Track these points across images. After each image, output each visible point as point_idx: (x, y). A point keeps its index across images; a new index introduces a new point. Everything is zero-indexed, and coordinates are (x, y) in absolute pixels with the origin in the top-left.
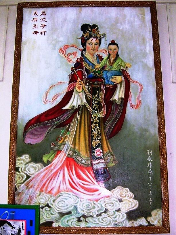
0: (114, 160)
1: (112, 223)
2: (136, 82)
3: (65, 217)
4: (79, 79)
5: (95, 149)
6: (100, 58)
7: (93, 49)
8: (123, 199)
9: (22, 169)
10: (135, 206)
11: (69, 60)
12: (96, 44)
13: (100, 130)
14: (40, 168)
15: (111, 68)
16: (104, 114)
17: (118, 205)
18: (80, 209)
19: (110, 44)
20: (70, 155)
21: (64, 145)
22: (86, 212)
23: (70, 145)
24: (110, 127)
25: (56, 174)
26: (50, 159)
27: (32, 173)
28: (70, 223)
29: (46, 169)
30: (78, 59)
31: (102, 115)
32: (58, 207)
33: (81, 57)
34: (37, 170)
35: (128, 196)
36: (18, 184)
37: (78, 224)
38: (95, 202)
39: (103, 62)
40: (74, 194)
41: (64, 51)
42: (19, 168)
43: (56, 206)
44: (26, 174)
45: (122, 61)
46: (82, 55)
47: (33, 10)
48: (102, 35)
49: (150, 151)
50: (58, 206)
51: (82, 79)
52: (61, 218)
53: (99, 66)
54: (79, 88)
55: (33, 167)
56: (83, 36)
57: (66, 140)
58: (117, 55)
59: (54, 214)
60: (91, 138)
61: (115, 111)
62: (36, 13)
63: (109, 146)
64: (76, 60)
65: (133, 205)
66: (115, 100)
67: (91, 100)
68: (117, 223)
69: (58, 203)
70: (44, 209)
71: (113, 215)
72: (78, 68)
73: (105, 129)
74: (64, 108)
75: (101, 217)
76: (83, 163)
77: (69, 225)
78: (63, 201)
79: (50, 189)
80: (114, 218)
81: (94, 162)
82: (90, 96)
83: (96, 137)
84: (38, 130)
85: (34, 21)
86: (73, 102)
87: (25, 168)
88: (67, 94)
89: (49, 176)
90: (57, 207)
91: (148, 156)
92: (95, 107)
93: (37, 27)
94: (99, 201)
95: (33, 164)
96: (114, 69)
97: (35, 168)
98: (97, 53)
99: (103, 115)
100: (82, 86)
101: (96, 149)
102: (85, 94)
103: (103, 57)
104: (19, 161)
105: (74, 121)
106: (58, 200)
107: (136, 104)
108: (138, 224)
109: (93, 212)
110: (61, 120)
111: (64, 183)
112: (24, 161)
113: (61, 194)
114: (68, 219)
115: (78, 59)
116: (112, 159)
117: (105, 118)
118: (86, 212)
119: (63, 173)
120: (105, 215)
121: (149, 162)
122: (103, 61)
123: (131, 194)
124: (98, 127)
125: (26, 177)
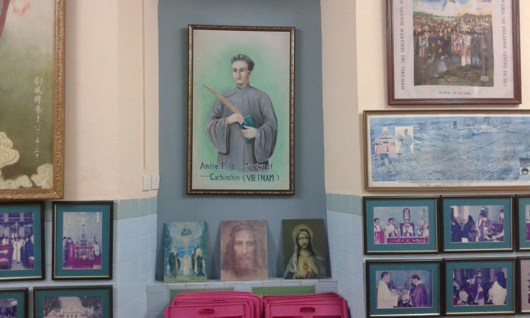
10: (13, 159)
35: (4, 144)
49: (39, 80)
65: (11, 158)
121: (37, 95)
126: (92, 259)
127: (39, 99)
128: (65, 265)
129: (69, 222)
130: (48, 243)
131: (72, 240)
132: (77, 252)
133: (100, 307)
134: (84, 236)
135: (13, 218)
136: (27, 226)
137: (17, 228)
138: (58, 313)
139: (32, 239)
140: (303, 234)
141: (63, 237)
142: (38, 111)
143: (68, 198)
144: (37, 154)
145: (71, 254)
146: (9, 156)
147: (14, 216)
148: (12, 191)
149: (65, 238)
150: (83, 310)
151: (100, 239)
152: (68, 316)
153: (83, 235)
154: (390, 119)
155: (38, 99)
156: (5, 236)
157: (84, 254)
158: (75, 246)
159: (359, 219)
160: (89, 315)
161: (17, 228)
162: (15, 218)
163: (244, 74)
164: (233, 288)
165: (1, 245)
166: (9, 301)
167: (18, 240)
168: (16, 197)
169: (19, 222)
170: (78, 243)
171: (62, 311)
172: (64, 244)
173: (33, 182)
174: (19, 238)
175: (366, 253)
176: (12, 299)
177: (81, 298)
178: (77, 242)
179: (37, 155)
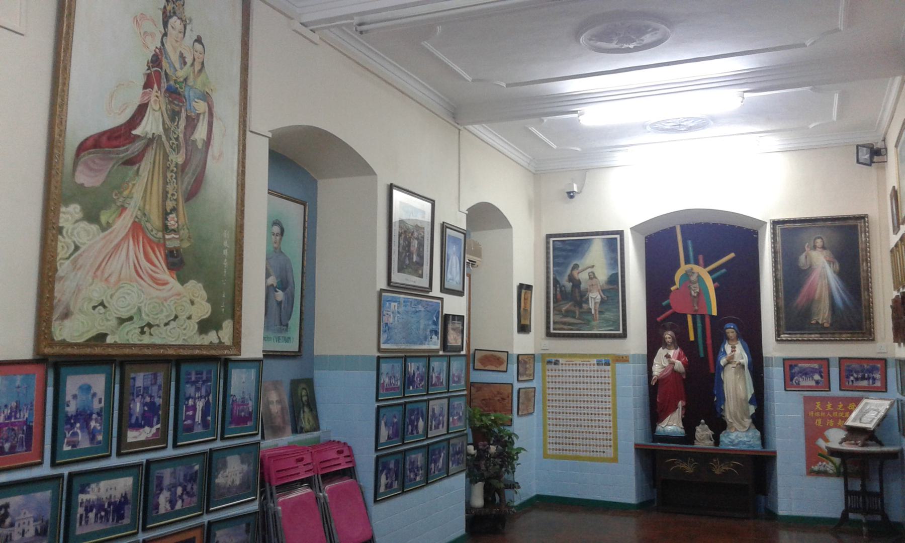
4: (156, 87)
10: (204, 315)
18: (145, 312)
21: (131, 198)
22: (153, 318)
25: (118, 246)
29: (105, 237)
31: (180, 159)
34: (91, 237)
36: (59, 260)
40: (140, 288)
44: (74, 242)
51: (159, 89)
52: (119, 327)
53: (181, 74)
55: (85, 230)
68: (185, 338)
73: (182, 184)
75: (168, 327)
76: (153, 235)
80: (184, 329)
81: (167, 237)
82: (167, 121)
86: (146, 125)
87: (73, 229)
89: (107, 251)
95: (84, 225)
116: (187, 236)
118: (153, 318)
125: (73, 247)
139: (211, 398)
140: (304, 393)
142: (225, 264)
154: (388, 296)
157: (243, 411)
159: (375, 373)
163: (278, 238)
164: (277, 445)
173: (219, 338)
174: (201, 397)
175: (377, 400)
179: (223, 310)
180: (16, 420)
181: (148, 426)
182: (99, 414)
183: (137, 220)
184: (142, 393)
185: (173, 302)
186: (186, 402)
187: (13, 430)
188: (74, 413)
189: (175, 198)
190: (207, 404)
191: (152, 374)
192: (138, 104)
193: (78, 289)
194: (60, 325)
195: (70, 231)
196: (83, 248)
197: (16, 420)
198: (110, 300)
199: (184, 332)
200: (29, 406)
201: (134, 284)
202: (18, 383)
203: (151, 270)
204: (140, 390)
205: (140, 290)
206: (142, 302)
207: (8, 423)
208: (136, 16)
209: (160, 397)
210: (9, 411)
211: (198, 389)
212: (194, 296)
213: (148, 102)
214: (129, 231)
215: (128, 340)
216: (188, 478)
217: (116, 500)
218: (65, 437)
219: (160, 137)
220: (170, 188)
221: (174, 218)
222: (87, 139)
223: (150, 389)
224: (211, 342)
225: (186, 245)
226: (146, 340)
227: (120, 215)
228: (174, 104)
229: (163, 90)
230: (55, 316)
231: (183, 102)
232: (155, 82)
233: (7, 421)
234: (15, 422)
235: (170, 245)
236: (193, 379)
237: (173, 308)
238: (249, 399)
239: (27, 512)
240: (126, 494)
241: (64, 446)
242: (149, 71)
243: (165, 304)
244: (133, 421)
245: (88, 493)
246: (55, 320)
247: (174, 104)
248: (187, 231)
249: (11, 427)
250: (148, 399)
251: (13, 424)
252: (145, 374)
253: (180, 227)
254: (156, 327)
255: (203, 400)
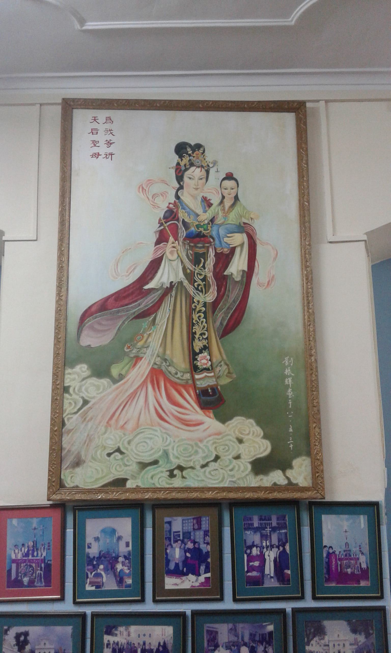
0: (229, 373)
1: (227, 479)
2: (267, 244)
3: (149, 470)
4: (171, 239)
5: (198, 354)
6: (207, 203)
7: (195, 187)
8: (245, 438)
9: (74, 389)
10: (265, 450)
11: (155, 206)
12: (201, 179)
13: (206, 322)
14: (106, 386)
15: (225, 220)
16: (214, 296)
17: (237, 449)
18: (173, 454)
19: (224, 179)
20: (157, 365)
21: (148, 347)
22: (184, 460)
23: (157, 347)
24: (223, 319)
25: (134, 394)
26: (123, 372)
27: (93, 396)
28: (155, 480)
29: (117, 388)
30: (170, 204)
31: (210, 297)
32: (137, 453)
33: (175, 201)
34: (101, 390)
35: (253, 433)
36: (67, 415)
37: (170, 482)
38: (199, 443)
39: (212, 211)
40: (164, 431)
41: (147, 190)
42: (69, 387)
43: (134, 452)
44: (83, 398)
45: (244, 208)
46: (177, 197)
47: (90, 113)
48: (212, 163)
49: (289, 359)
50: (136, 452)
51: (176, 239)
52: (141, 472)
53: (205, 217)
54: (172, 253)
55: (94, 385)
56: (178, 164)
57: (150, 340)
58: (236, 198)
59: (129, 466)
60: (192, 337)
61: (232, 293)
62: (95, 120)
63: (222, 350)
64: (167, 206)
65: (262, 449)
66: (232, 274)
67: (193, 273)
68: (234, 479)
69: (136, 447)
70: (112, 456)
71: (227, 466)
72: (169, 219)
73: (214, 322)
74: (146, 287)
75: (207, 469)
76: (178, 378)
77: (154, 484)
78: (145, 442)
79: (124, 422)
80: (231, 470)
81: (197, 377)
82: (189, 265)
83: (200, 335)
84: (103, 323)
85: (93, 134)
86: (161, 277)
87: (81, 387)
88: (152, 262)
89: (122, 400)
90: (136, 454)
91: (287, 367)
92: (199, 285)
93: (97, 145)
94: (205, 441)
95: (94, 380)
96: (230, 222)
97: (98, 387)
98: (202, 194)
99: (212, 299)
100: (177, 250)
101: (200, 355)
102: (182, 264)
103: (211, 202)
104: (69, 376)
105: (164, 310)
106: (137, 440)
107: (267, 280)
108: (271, 482)
109: (195, 460)
110: (142, 306)
111: (147, 411)
112: (78, 376)
113: (142, 431)
114: (153, 473)
115: (170, 204)
116: (227, 371)
117: (215, 304)
118: (184, 460)
119: (145, 394)
120: (215, 465)
121: (288, 377)
122: (212, 208)
123: (259, 431)
124: (203, 318)
125: (81, 402)
126: (358, 573)
127: (290, 381)
128: (328, 580)
129: (329, 527)
130: (304, 553)
131: (334, 550)
132: (340, 565)
133: (372, 634)
134: (347, 544)
135: (264, 522)
136: (281, 531)
137: (269, 534)
138: (322, 642)
139: (287, 547)
141: (323, 546)
142: (290, 394)
143: (328, 499)
144: (291, 444)
145: (333, 567)
146: (259, 447)
147: (265, 519)
148: (266, 489)
149: (325, 546)
150: (351, 637)
151: (366, 549)
152: (334, 645)
153: (347, 544)
155: (289, 381)
156: (255, 544)
157: (349, 567)
158: (338, 557)
160: (359, 644)
161: (269, 534)
162: (266, 522)
165: (251, 555)
166: (264, 625)
167: (270, 549)
168: (271, 496)
169: (270, 526)
170: (341, 553)
171: (327, 638)
172: (325, 555)
173: (288, 478)
174: (272, 546)
176: (267, 623)
177: (349, 622)
178: (340, 552)
179: (291, 446)
180: (33, 558)
181: (193, 574)
182: (125, 557)
183: (156, 367)
184: (181, 538)
185: (211, 442)
186: (248, 551)
187: (31, 566)
188: (97, 555)
189: (205, 337)
190: (283, 554)
191: (194, 519)
192: (150, 260)
193: (90, 439)
194: (71, 473)
195: (76, 389)
196: (92, 402)
197: (33, 558)
198: (127, 445)
199: (232, 473)
200: (46, 547)
201: (157, 428)
202: (34, 525)
203: (179, 413)
204: (179, 536)
205: (165, 433)
206: (169, 444)
207: (25, 560)
208: (142, 185)
209: (208, 544)
210: (26, 550)
211: (264, 537)
212: (242, 434)
213: (162, 256)
214: (147, 377)
215: (154, 484)
216: (257, 638)
217: (152, 648)
218: (87, 577)
219: (181, 283)
220: (198, 330)
221: (206, 357)
222: (90, 307)
223: (192, 534)
224: (275, 484)
225: (225, 381)
226: (177, 483)
227: (135, 365)
228: (198, 247)
229: (181, 240)
230: (64, 466)
231: (210, 242)
232: (170, 235)
233: (24, 558)
234: (33, 560)
235: (202, 384)
236: (256, 525)
237: (212, 449)
238: (358, 552)
239: (47, 643)
240: (165, 643)
241: (87, 585)
242: (162, 227)
243: (201, 445)
244: (172, 566)
245: (116, 635)
246: (66, 469)
247: (198, 247)
248: (226, 367)
249: (29, 564)
250: (190, 545)
251: (29, 561)
252: (185, 518)
253: (214, 366)
254: (189, 470)
255: (275, 550)
